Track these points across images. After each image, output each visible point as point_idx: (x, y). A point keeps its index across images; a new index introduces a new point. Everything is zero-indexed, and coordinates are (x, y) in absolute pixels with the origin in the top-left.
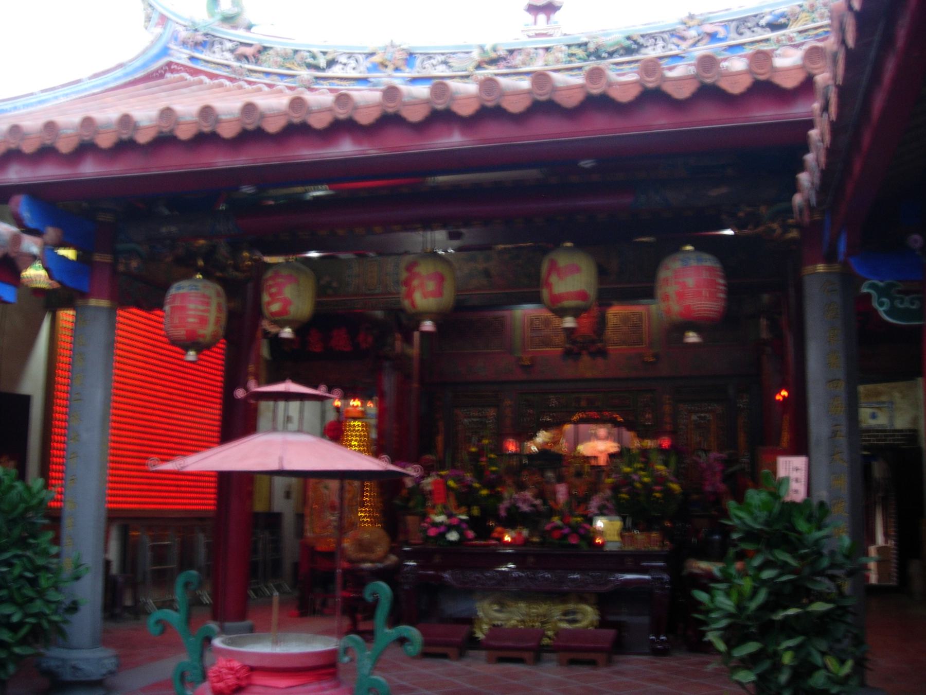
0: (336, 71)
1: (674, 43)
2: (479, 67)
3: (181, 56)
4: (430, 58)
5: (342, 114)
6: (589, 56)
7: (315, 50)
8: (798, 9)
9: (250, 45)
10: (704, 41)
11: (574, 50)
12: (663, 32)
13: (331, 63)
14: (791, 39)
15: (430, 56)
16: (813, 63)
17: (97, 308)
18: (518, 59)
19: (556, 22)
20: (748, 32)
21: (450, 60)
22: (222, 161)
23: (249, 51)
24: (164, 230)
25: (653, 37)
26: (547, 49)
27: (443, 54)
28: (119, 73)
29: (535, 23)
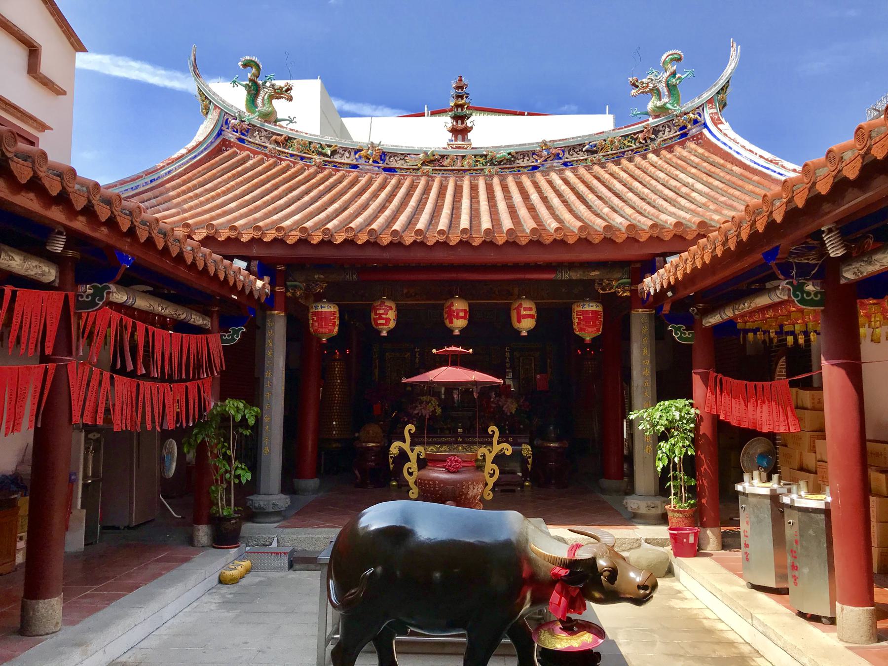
0: (337, 159)
1: (534, 159)
2: (423, 164)
6: (486, 163)
7: (323, 143)
9: (281, 135)
12: (529, 151)
13: (334, 153)
14: (600, 160)
18: (446, 162)
20: (575, 155)
22: (709, 282)
24: (316, 277)
26: (463, 157)
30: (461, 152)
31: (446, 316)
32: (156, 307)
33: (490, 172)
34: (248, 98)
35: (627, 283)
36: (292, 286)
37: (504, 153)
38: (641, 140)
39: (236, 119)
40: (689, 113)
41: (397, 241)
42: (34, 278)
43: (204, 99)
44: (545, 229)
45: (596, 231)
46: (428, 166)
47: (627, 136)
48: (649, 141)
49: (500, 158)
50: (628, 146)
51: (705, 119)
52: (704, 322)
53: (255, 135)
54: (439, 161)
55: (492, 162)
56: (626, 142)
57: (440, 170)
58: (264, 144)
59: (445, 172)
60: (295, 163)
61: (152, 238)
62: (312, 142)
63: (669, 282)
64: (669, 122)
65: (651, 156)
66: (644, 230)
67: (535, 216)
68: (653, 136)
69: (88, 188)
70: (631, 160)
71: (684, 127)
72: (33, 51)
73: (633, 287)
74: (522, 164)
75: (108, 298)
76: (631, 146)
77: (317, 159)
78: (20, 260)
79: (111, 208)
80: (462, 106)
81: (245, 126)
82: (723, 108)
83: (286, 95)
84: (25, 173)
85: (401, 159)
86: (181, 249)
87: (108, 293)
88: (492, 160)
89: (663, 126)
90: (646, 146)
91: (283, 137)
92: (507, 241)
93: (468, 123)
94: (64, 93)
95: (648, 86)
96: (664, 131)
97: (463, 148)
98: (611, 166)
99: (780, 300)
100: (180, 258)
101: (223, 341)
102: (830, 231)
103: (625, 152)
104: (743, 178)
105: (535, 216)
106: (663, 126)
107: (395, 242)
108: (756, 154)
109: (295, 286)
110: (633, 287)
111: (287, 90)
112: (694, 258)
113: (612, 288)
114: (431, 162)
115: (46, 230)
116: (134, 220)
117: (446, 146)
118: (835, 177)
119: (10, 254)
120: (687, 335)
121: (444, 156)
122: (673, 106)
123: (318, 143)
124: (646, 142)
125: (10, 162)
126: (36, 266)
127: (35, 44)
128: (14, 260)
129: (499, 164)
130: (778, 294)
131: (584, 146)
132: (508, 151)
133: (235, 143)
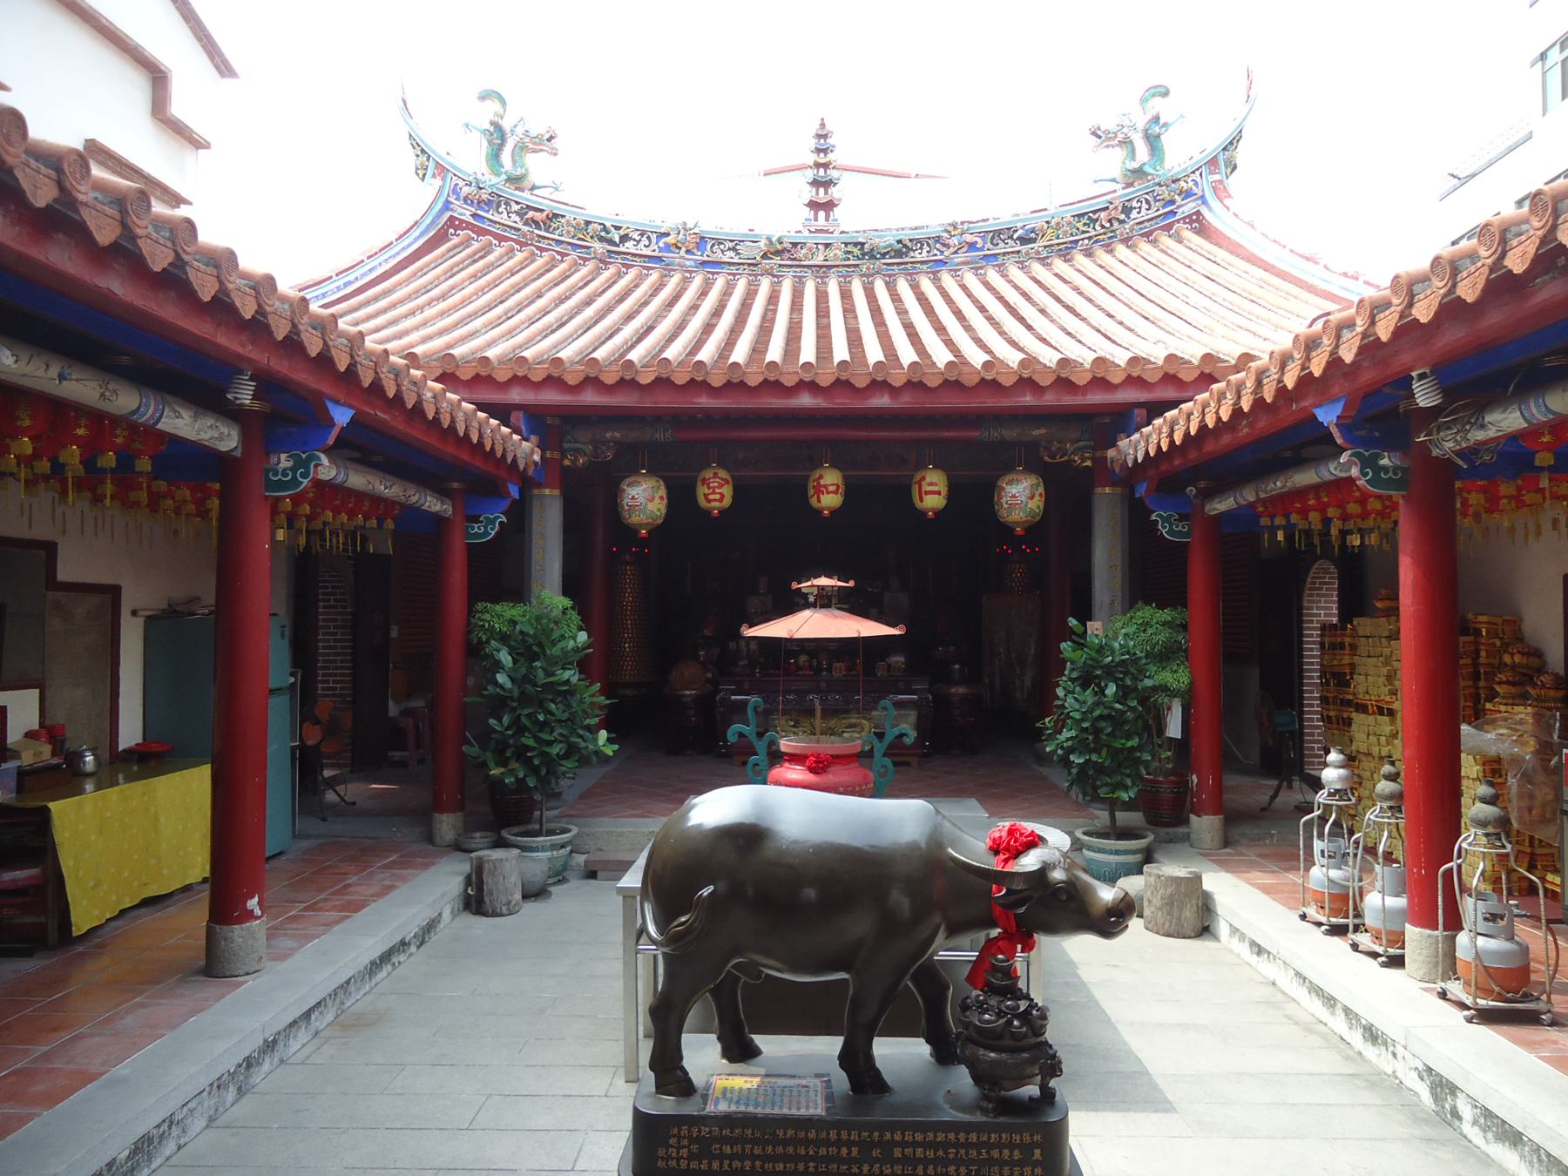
0: (629, 246)
2: (765, 256)
3: (465, 213)
4: (720, 243)
5: (807, 377)
6: (864, 254)
7: (608, 224)
8: (1046, 226)
9: (542, 211)
10: (964, 250)
11: (850, 248)
12: (929, 238)
13: (625, 238)
15: (719, 242)
16: (1133, 368)
17: (551, 496)
19: (836, 220)
20: (1002, 245)
21: (738, 247)
23: (538, 216)
24: (608, 435)
25: (920, 242)
26: (827, 246)
27: (732, 241)
28: (416, 232)
29: (816, 219)
30: (822, 238)
31: (811, 492)
32: (377, 485)
33: (868, 268)
34: (490, 152)
35: (1086, 447)
36: (572, 450)
37: (891, 240)
38: (1104, 223)
39: (470, 185)
40: (1179, 180)
41: (738, 380)
42: (207, 443)
43: (419, 153)
44: (967, 364)
45: (1045, 366)
46: (772, 259)
47: (1083, 215)
48: (1116, 224)
49: (885, 248)
50: (1084, 232)
51: (1203, 190)
52: (1207, 508)
53: (500, 210)
54: (789, 251)
55: (872, 255)
56: (1080, 225)
57: (791, 266)
58: (515, 225)
59: (799, 270)
60: (563, 255)
61: (380, 379)
62: (591, 222)
63: (1159, 447)
64: (1147, 193)
65: (1121, 250)
66: (1119, 366)
67: (949, 343)
68: (1122, 217)
69: (291, 305)
70: (1088, 253)
71: (1172, 202)
72: (157, 78)
73: (1098, 454)
74: (919, 258)
75: (316, 472)
76: (1088, 232)
77: (599, 247)
78: (190, 417)
79: (322, 334)
80: (826, 166)
81: (484, 197)
82: (1231, 173)
83: (547, 146)
84: (209, 285)
85: (729, 249)
86: (419, 396)
87: (316, 466)
88: (872, 250)
89: (1138, 201)
90: (1112, 232)
91: (545, 214)
92: (909, 381)
93: (835, 192)
94: (206, 146)
95: (1116, 137)
96: (1140, 208)
97: (827, 232)
98: (1059, 265)
99: (1332, 478)
100: (418, 409)
101: (469, 536)
102: (1422, 377)
103: (1078, 241)
104: (1263, 285)
105: (949, 343)
106: (1138, 201)
107: (735, 381)
108: (1284, 247)
109: (577, 450)
110: (1098, 454)
111: (549, 140)
112: (1203, 410)
113: (1065, 454)
114: (777, 253)
115: (230, 368)
116: (354, 354)
117: (801, 228)
118: (1445, 296)
119: (177, 408)
120: (1180, 528)
121: (797, 244)
122: (1154, 169)
123: (600, 224)
124: (1112, 225)
125: (188, 268)
126: (211, 426)
127: (162, 68)
128: (182, 418)
129: (884, 258)
130: (1332, 469)
131: (1016, 231)
132: (898, 238)
133: (468, 223)
